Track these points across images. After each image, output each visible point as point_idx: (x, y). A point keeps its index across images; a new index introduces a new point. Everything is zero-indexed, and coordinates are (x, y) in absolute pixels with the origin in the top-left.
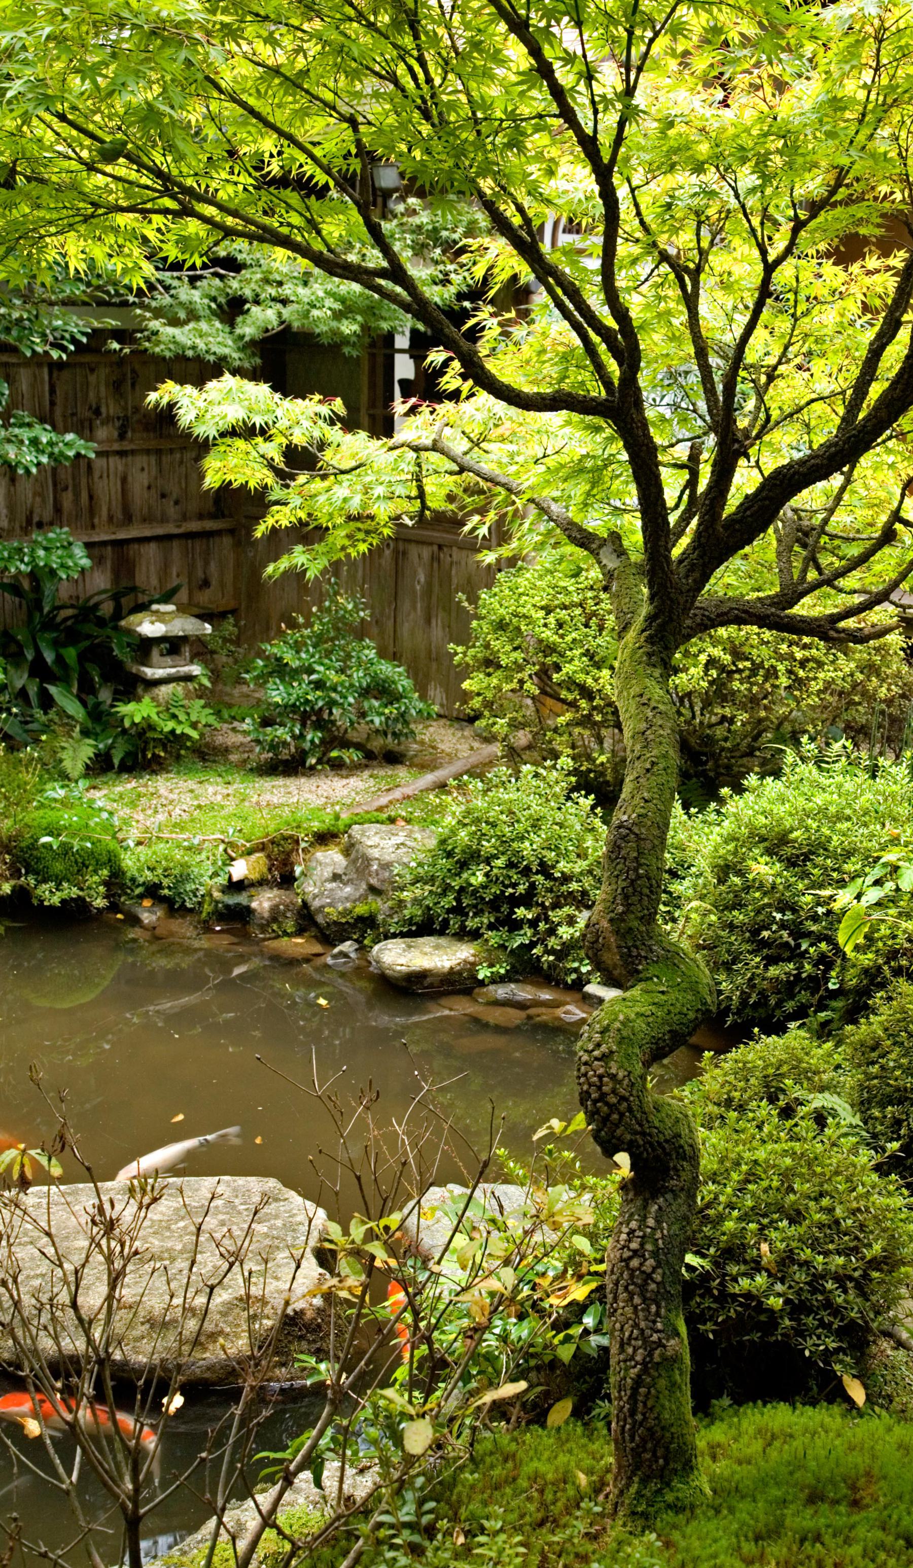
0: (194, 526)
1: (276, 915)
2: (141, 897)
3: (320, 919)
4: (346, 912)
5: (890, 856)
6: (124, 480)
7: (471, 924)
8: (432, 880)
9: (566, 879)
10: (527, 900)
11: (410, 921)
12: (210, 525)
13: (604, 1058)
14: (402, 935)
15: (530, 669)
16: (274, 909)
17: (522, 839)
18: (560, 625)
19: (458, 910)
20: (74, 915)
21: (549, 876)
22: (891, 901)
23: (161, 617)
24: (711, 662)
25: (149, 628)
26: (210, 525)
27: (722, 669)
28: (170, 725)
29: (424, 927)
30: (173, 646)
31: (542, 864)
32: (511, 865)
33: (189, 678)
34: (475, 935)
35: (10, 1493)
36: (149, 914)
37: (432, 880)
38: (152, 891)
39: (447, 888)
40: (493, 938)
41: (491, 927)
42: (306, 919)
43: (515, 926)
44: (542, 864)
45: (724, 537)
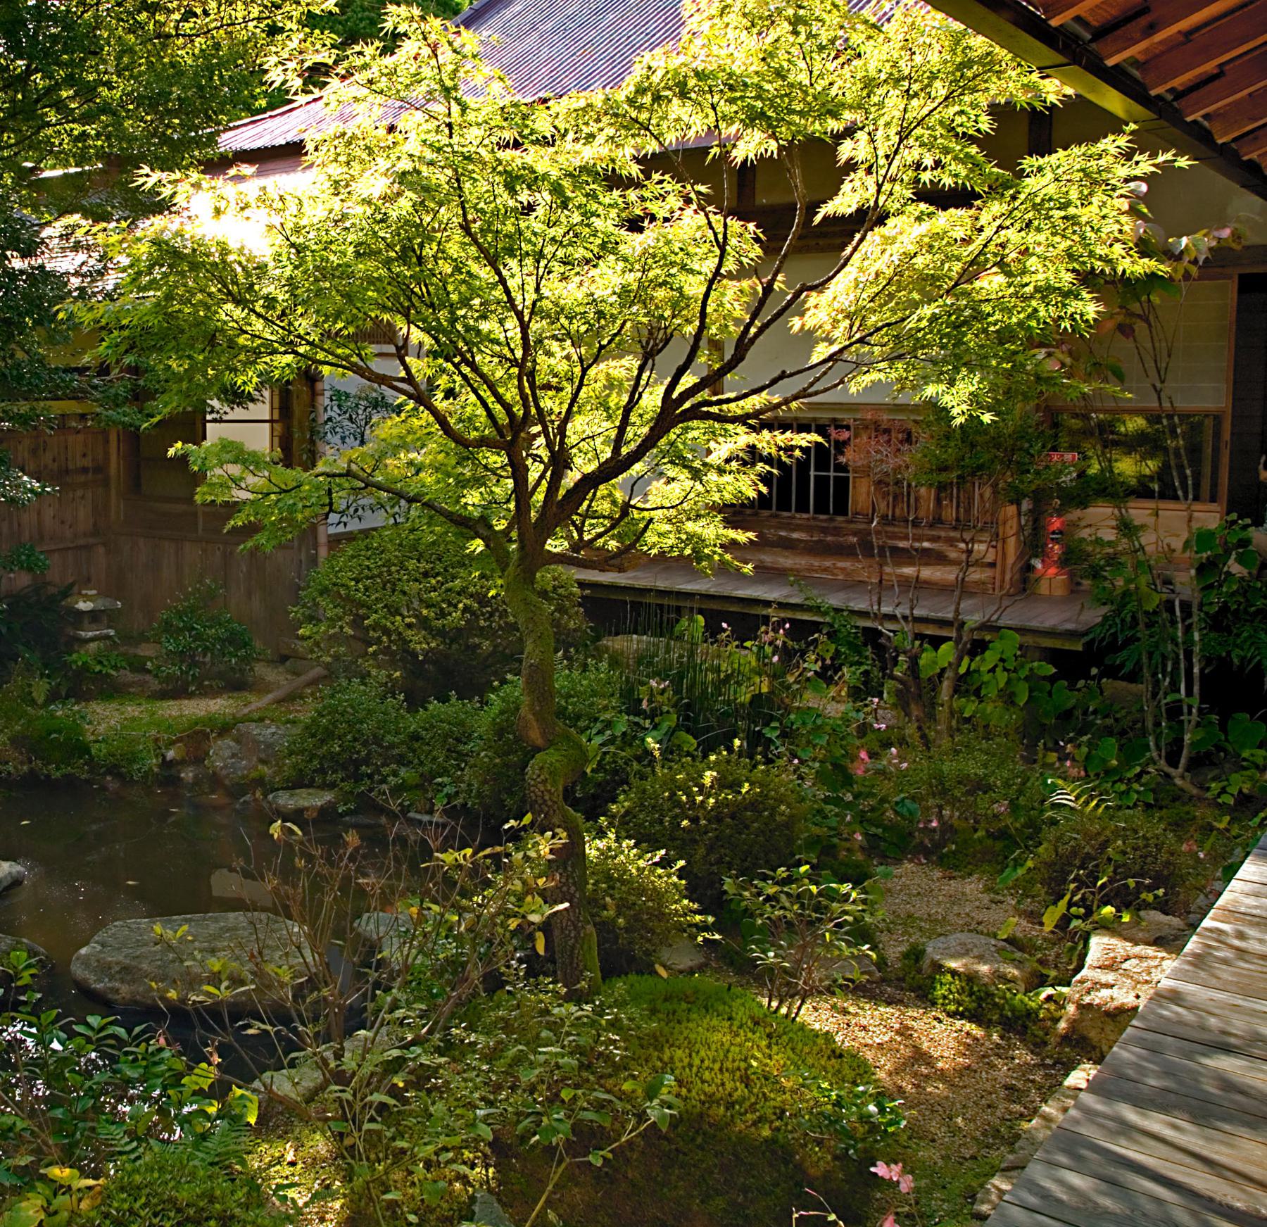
0: (82, 542)
1: (197, 782)
2: (105, 774)
3: (227, 782)
4: (243, 777)
5: (607, 716)
6: (39, 514)
7: (330, 778)
8: (302, 752)
9: (392, 746)
10: (366, 761)
11: (287, 781)
12: (91, 540)
13: (544, 782)
14: (287, 788)
15: (348, 618)
16: (196, 776)
17: (361, 723)
18: (367, 589)
19: (322, 771)
20: (70, 783)
21: (380, 746)
22: (612, 741)
23: (88, 598)
24: (466, 609)
25: (83, 606)
26: (91, 540)
27: (473, 613)
28: (98, 668)
29: (297, 783)
30: (94, 616)
31: (375, 736)
32: (355, 740)
33: (108, 637)
34: (332, 786)
35: (236, 1051)
36: (111, 782)
37: (302, 752)
38: (114, 770)
39: (313, 757)
40: (347, 786)
41: (343, 780)
42: (215, 781)
43: (358, 778)
44: (375, 736)
45: (547, 526)
